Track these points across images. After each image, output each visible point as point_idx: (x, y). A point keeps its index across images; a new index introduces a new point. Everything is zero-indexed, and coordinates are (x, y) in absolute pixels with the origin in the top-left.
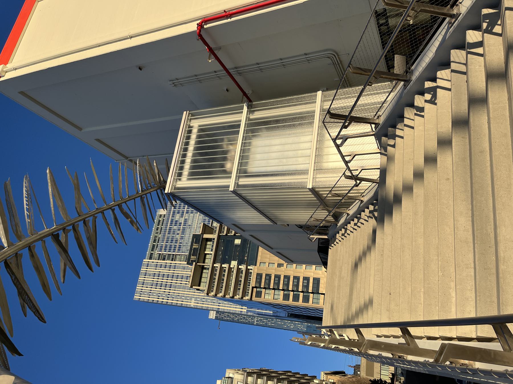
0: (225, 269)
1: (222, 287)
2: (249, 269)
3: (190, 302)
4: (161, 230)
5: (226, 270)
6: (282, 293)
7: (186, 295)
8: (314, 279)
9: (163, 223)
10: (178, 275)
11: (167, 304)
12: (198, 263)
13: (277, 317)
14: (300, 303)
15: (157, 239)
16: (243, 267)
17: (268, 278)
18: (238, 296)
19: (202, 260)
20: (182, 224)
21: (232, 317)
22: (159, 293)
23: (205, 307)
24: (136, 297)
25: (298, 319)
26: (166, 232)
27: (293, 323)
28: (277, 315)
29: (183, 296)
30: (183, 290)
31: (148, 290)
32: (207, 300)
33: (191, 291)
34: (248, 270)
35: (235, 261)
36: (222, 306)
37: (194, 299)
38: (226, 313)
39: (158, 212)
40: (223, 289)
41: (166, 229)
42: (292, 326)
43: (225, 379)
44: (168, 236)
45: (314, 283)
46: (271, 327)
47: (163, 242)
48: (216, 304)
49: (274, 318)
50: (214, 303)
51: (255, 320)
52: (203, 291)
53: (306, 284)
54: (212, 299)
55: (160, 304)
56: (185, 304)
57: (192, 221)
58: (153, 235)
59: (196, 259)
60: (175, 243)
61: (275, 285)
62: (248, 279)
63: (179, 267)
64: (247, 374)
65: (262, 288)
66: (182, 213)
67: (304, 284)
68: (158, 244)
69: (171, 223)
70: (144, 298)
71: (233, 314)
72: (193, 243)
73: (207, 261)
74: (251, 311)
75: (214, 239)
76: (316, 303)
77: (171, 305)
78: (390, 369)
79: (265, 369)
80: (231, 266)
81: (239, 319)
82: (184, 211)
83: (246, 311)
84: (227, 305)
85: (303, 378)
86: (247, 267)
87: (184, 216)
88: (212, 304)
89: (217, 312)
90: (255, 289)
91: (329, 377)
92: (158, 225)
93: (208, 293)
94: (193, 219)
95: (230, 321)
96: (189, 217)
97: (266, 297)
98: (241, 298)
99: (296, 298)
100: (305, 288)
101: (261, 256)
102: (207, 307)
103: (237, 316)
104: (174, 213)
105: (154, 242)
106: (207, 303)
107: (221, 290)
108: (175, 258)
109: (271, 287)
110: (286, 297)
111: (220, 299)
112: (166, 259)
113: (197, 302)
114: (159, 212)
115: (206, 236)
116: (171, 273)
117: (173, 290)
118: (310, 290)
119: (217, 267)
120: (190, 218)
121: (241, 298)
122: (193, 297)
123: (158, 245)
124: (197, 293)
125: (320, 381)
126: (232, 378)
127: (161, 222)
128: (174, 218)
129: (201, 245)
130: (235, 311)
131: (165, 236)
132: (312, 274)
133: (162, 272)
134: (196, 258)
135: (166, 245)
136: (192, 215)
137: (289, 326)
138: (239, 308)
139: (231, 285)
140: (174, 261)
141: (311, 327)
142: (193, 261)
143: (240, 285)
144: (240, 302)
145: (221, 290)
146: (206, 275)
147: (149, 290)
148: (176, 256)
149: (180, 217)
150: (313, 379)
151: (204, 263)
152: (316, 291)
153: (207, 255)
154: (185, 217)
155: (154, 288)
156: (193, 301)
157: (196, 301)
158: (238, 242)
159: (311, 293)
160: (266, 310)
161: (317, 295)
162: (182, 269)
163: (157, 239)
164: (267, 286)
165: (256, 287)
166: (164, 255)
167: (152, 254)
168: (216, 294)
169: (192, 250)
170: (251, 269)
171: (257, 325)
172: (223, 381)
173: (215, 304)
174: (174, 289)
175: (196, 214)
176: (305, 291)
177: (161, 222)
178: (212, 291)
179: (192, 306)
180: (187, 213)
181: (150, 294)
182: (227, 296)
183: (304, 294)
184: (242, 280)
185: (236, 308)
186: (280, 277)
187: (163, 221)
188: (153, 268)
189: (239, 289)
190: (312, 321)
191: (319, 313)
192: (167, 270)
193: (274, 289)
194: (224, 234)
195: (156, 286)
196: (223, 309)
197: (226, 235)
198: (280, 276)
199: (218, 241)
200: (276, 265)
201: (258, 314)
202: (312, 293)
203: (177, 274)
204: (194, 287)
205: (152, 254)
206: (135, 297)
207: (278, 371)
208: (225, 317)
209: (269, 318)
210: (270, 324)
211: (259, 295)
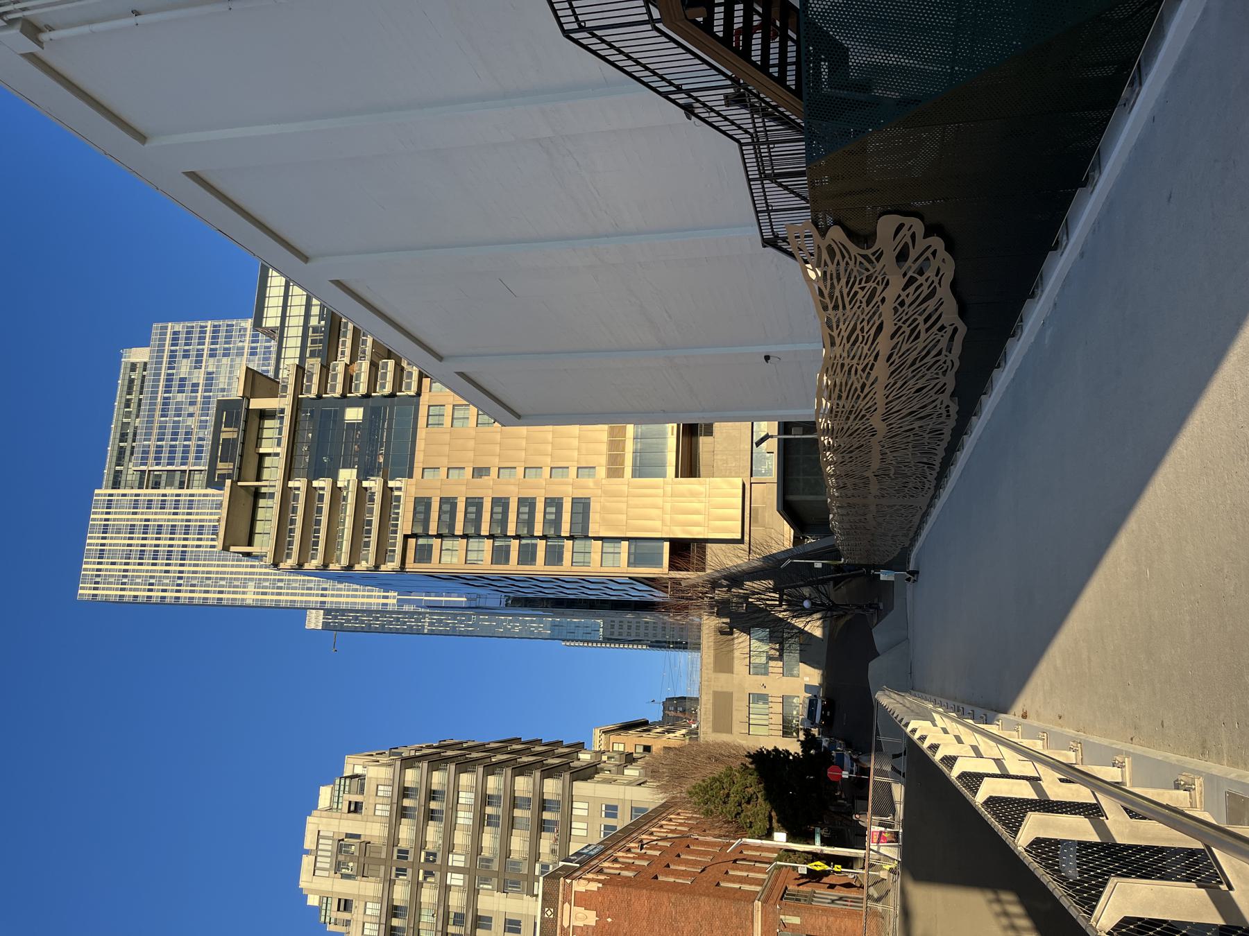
0: (321, 492)
1: (316, 544)
3: (244, 593)
4: (139, 405)
5: (324, 494)
6: (488, 544)
8: (575, 501)
9: (142, 387)
13: (480, 610)
14: (540, 567)
15: (130, 431)
16: (374, 484)
17: (446, 507)
18: (364, 563)
19: (251, 469)
20: (200, 388)
21: (366, 620)
22: (152, 577)
23: (286, 601)
24: (85, 592)
25: (533, 610)
26: (154, 410)
27: (518, 621)
28: (478, 605)
29: (222, 579)
31: (116, 570)
32: (275, 584)
33: (242, 563)
34: (389, 491)
35: (350, 470)
37: (251, 584)
39: (125, 358)
40: (321, 547)
42: (517, 626)
43: (343, 781)
45: (574, 511)
46: (465, 634)
47: (149, 440)
51: (424, 622)
52: (258, 557)
53: (553, 517)
54: (304, 581)
56: (228, 599)
58: (117, 420)
59: (233, 469)
61: (469, 525)
62: (390, 516)
63: (202, 504)
65: (432, 536)
67: (547, 516)
68: (134, 444)
70: (110, 592)
72: (221, 427)
73: (266, 474)
74: (409, 602)
75: (282, 411)
76: (582, 564)
78: (771, 710)
79: (452, 742)
80: (340, 484)
81: (385, 625)
82: (203, 350)
84: (346, 593)
85: (551, 753)
87: (204, 364)
89: (328, 612)
90: (412, 542)
91: (613, 738)
92: (129, 393)
95: (362, 630)
96: (218, 367)
97: (446, 559)
98: (373, 569)
99: (527, 555)
100: (550, 527)
101: (424, 451)
102: (291, 601)
103: (379, 617)
104: (173, 356)
108: (189, 480)
109: (459, 530)
110: (500, 555)
111: (339, 578)
112: (163, 483)
114: (129, 357)
115: (256, 404)
116: (182, 521)
117: (190, 565)
118: (565, 532)
120: (223, 370)
121: (373, 569)
122: (250, 579)
123: (133, 448)
124: (245, 567)
126: (360, 776)
127: (137, 383)
128: (174, 371)
129: (245, 431)
131: (152, 422)
133: (155, 520)
134: (232, 467)
135: (158, 446)
137: (510, 629)
138: (379, 597)
139: (343, 534)
140: (188, 488)
141: (562, 626)
142: (223, 477)
143: (369, 532)
144: (372, 579)
146: (268, 512)
147: (120, 570)
148: (190, 474)
149: (190, 366)
150: (577, 752)
151: (258, 479)
152: (581, 534)
154: (207, 367)
155: (134, 564)
156: (251, 587)
157: (259, 588)
158: (354, 414)
159: (567, 538)
160: (449, 594)
162: (212, 508)
164: (445, 531)
166: (156, 473)
167: (117, 474)
169: (219, 444)
170: (399, 489)
171: (431, 633)
172: (337, 788)
177: (137, 383)
178: (289, 556)
179: (249, 602)
180: (212, 356)
182: (332, 567)
183: (549, 543)
184: (373, 518)
187: (143, 382)
189: (367, 545)
191: (588, 588)
192: (169, 514)
193: (465, 536)
197: (319, 397)
199: (294, 418)
200: (469, 471)
201: (429, 607)
202: (571, 538)
204: (233, 549)
205: (117, 474)
206: (80, 591)
207: (486, 742)
208: (348, 621)
209: (460, 614)
210: (463, 627)
211: (424, 554)
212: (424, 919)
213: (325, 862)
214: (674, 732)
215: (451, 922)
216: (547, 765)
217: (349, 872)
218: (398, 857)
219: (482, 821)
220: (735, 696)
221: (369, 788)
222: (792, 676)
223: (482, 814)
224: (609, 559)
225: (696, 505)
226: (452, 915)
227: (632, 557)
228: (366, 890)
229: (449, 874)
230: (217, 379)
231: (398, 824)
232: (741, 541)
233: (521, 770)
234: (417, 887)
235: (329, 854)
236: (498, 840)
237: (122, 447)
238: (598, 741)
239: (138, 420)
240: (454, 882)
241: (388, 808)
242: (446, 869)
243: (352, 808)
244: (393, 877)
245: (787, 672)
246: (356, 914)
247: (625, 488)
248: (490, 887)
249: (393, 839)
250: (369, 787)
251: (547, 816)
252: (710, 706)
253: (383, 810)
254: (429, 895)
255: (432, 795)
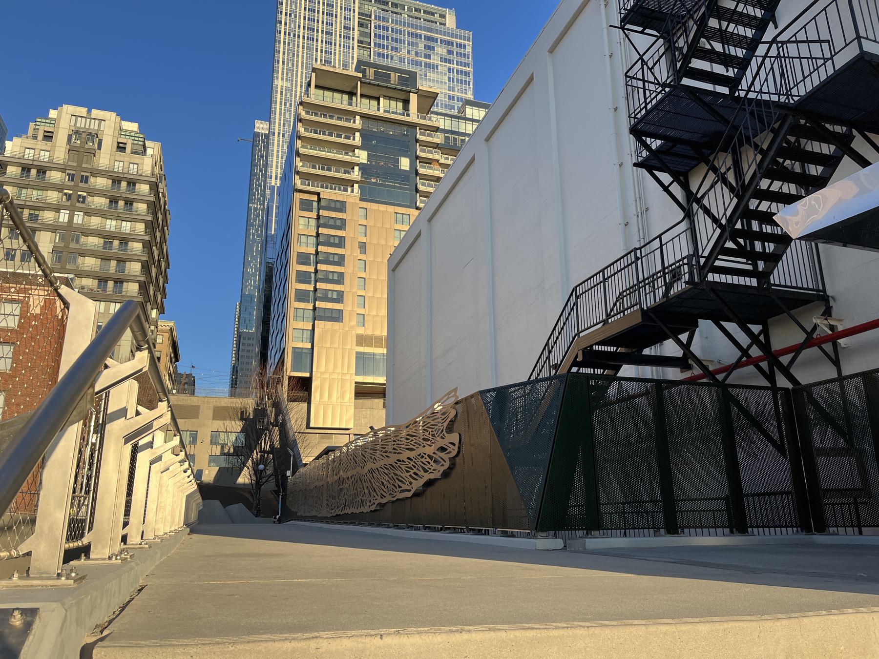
1: (316, 132)
2: (353, 186)
3: (282, 79)
4: (416, 18)
7: (295, 69)
9: (428, 21)
10: (331, 54)
11: (275, 31)
12: (361, 82)
13: (265, 243)
14: (294, 286)
15: (399, 10)
16: (356, 174)
17: (339, 223)
18: (301, 164)
19: (366, 92)
20: (427, 60)
22: (295, 16)
23: (276, 108)
26: (413, 27)
27: (256, 271)
29: (293, 65)
30: (305, 64)
35: (366, 158)
36: (279, 141)
38: (267, 153)
40: (313, 135)
41: (417, 28)
42: (252, 271)
43: (142, 140)
44: (404, 31)
47: (392, 22)
48: (282, 129)
49: (262, 238)
50: (284, 125)
51: (257, 204)
53: (330, 296)
54: (290, 122)
55: (276, 26)
57: (433, 80)
59: (369, 79)
60: (392, 47)
63: (346, 55)
64: (153, 183)
66: (449, 60)
67: (330, 292)
68: (390, 12)
69: (429, 38)
71: (266, 166)
73: (365, 101)
75: (408, 115)
77: (274, 41)
82: (453, 64)
83: (273, 184)
85: (157, 289)
86: (357, 182)
87: (443, 63)
88: (280, 152)
89: (267, 136)
90: (315, 198)
91: (167, 335)
93: (304, 104)
94: (437, 81)
95: (253, 160)
96: (441, 73)
97: (302, 221)
98: (297, 170)
99: (303, 277)
100: (323, 294)
104: (450, 43)
105: (392, 3)
106: (283, 111)
107: (311, 130)
108: (364, 47)
110: (303, 259)
111: (291, 146)
112: (362, 29)
113: (284, 91)
114: (449, 14)
115: (414, 98)
117: (303, 43)
119: (354, 122)
120: (440, 76)
121: (297, 170)
122: (292, 84)
124: (301, 81)
125: (155, 320)
127: (431, 18)
128: (439, 43)
130: (272, 165)
131: (405, 26)
132: (349, 309)
133: (336, 21)
134: (370, 78)
135: (388, 28)
136: (445, 79)
137: (250, 265)
138: (277, 173)
140: (358, 46)
142: (364, 72)
143: (323, 169)
144: (289, 170)
145: (311, 130)
146: (339, 101)
148: (368, 48)
151: (362, 96)
152: (317, 315)
153: (376, 103)
156: (286, 84)
157: (286, 90)
160: (277, 222)
161: (311, 316)
162: (343, 61)
163: (399, 10)
164: (322, 221)
165: (319, 200)
166: (369, 25)
168: (302, 138)
169: (387, 71)
170: (352, 191)
172: (137, 135)
173: (282, 127)
174: (305, 45)
175: (446, 87)
176: (316, 295)
177: (431, 18)
178: (307, 113)
179: (276, 82)
180: (449, 69)
181: (290, 64)
182: (299, 142)
184: (332, 172)
185: (277, 167)
186: (341, 248)
187: (432, 22)
188: (343, 3)
189: (314, 167)
190: (262, 306)
193: (318, 235)
194: (418, 136)
195: (309, 9)
196: (273, 143)
197: (417, 141)
198: (343, 246)
200: (364, 240)
202: (315, 308)
203: (333, 51)
204: (314, 75)
207: (167, 243)
208: (260, 151)
211: (306, 206)
212: (35, 192)
213: (81, 123)
214: (169, 379)
215: (32, 212)
216: (149, 286)
217: (73, 140)
218: (82, 176)
219: (108, 237)
220: (196, 421)
221: (133, 158)
222: (210, 462)
223: (114, 238)
224: (298, 334)
225: (335, 396)
226: (37, 212)
227: (300, 351)
228: (60, 154)
229: (68, 212)
230: (433, 72)
231: (108, 177)
232: (308, 427)
233: (146, 267)
234: (59, 188)
235: (87, 127)
236: (93, 248)
237: (388, 3)
238: (165, 324)
239: (406, 16)
240: (62, 215)
241: (120, 171)
242: (72, 210)
243: (121, 145)
244: (68, 171)
245: (212, 459)
246: (41, 144)
247: (349, 347)
248: (57, 241)
249: (96, 173)
250: (136, 158)
251: (111, 284)
252: (189, 403)
253: (119, 167)
254: (53, 196)
255: (129, 203)
